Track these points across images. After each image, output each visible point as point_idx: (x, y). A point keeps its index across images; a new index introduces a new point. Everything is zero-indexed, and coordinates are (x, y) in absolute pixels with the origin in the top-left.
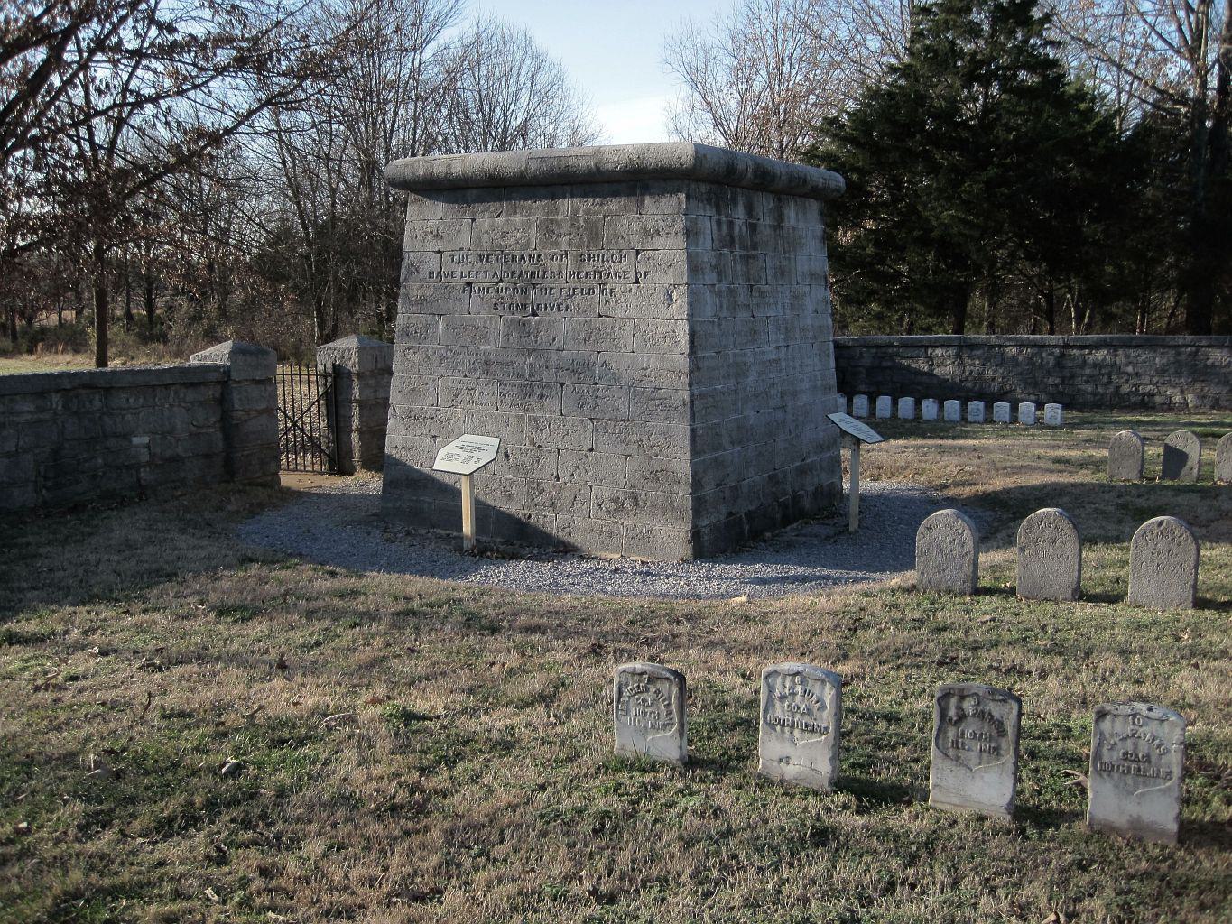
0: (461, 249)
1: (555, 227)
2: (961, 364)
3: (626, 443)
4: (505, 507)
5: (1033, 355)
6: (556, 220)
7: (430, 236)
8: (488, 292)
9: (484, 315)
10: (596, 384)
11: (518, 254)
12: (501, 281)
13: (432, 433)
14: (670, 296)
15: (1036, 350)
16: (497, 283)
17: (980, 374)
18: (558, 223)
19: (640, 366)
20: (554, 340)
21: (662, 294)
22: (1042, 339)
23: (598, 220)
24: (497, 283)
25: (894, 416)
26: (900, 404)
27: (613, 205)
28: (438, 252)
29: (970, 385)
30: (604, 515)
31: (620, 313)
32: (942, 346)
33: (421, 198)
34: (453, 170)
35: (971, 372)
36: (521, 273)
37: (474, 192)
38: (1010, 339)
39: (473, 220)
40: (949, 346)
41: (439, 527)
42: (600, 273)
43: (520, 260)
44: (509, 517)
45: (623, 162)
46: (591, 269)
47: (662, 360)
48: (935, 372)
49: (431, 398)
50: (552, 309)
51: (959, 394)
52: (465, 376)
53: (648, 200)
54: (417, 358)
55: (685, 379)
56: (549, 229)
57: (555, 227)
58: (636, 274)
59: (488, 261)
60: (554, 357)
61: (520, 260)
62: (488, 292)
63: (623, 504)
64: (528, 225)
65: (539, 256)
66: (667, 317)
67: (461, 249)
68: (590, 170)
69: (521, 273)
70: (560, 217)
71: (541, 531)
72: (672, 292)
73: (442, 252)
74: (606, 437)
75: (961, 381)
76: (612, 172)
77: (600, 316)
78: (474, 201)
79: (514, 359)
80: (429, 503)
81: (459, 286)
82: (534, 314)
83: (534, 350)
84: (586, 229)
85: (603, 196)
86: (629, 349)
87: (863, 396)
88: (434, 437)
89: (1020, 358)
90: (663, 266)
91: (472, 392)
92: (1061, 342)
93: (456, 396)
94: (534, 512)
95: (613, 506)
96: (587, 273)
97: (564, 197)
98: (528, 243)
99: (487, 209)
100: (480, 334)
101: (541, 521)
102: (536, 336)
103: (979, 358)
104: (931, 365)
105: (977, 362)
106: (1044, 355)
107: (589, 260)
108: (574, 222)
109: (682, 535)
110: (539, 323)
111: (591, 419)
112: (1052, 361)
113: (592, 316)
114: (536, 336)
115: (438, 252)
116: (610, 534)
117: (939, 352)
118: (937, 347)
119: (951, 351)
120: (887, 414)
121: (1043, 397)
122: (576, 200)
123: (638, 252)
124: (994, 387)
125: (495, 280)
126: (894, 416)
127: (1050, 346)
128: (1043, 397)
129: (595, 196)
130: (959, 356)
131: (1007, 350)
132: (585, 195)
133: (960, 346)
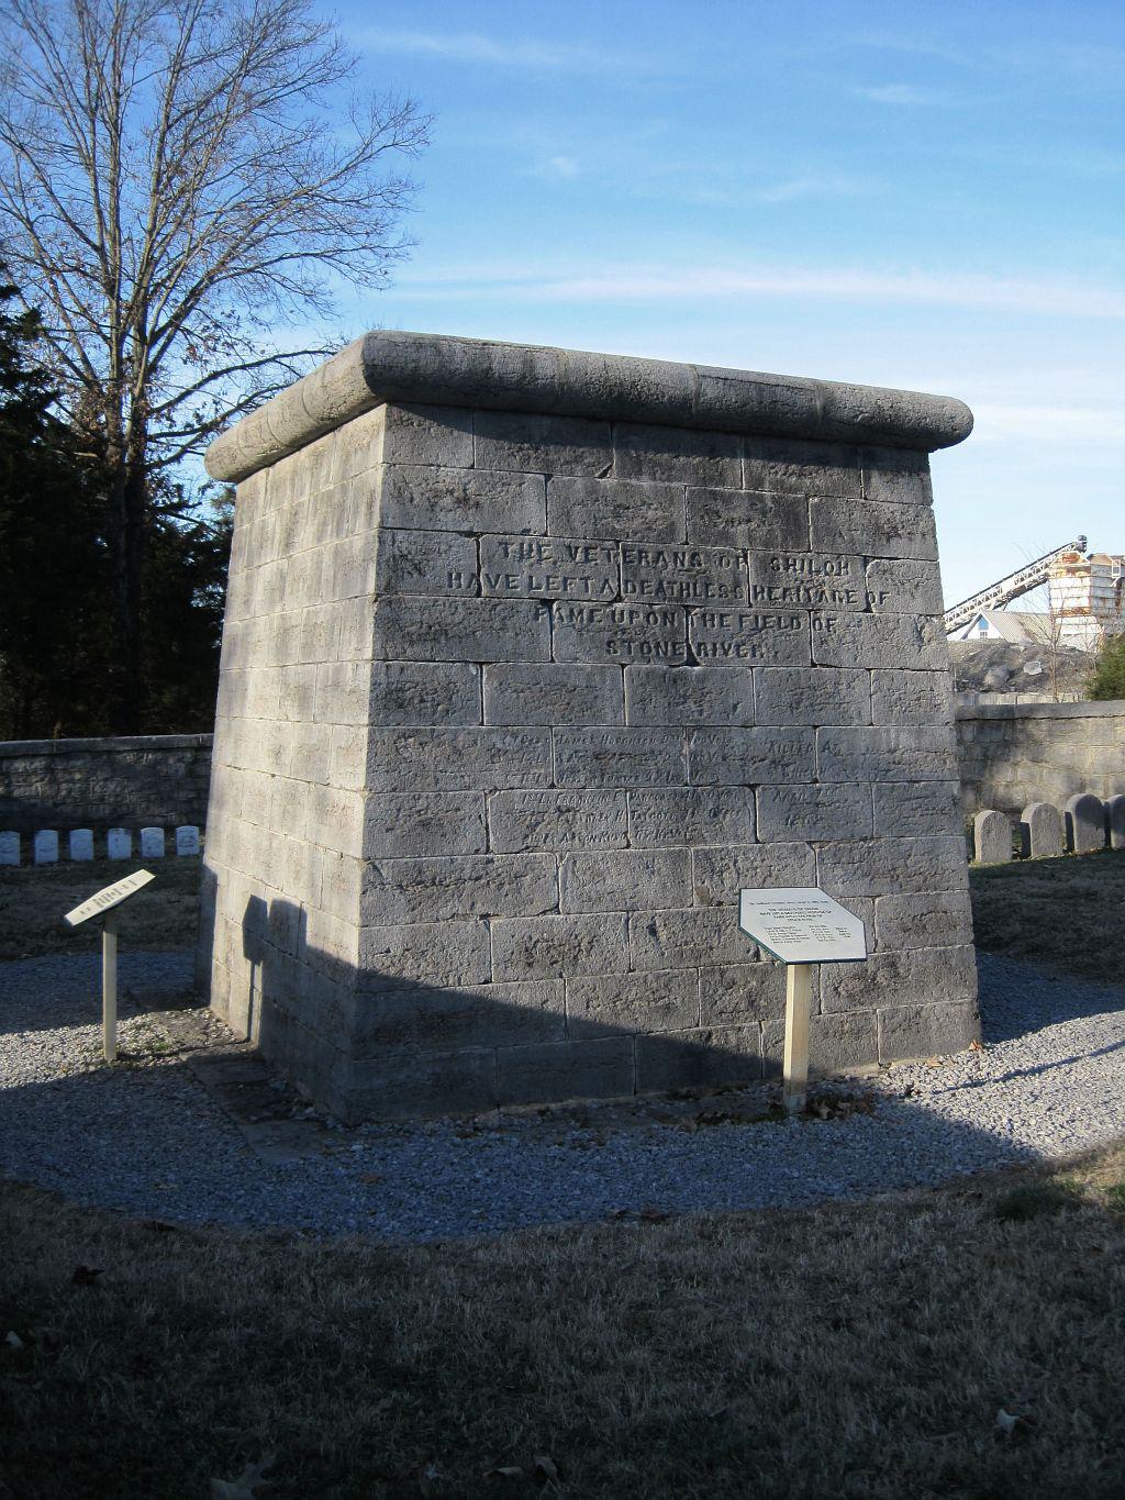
0: (526, 532)
1: (720, 506)
2: (54, 781)
3: (870, 875)
4: (659, 1028)
5: (157, 762)
6: (722, 495)
7: (447, 501)
8: (591, 619)
9: (586, 664)
10: (816, 781)
11: (651, 548)
12: (619, 599)
13: (480, 909)
14: (920, 633)
15: (159, 756)
16: (610, 603)
17: (83, 792)
18: (727, 499)
19: (884, 747)
20: (735, 707)
21: (909, 631)
22: (168, 739)
23: (796, 501)
24: (610, 603)
25: (64, 858)
26: (73, 840)
27: (822, 478)
28: (470, 534)
29: (69, 809)
30: (842, 1002)
31: (846, 658)
32: (25, 756)
33: (416, 419)
34: (539, 371)
35: (70, 791)
36: (661, 584)
37: (546, 422)
38: (124, 742)
39: (548, 477)
40: (35, 756)
41: (512, 1100)
42: (807, 590)
43: (656, 561)
44: (667, 1044)
45: (868, 410)
46: (792, 584)
47: (919, 733)
48: (16, 793)
49: (470, 837)
50: (726, 653)
51: (52, 824)
52: (552, 786)
53: (876, 479)
54: (430, 755)
55: (951, 764)
56: (708, 503)
57: (720, 506)
58: (867, 597)
59: (587, 560)
60: (738, 740)
61: (656, 561)
62: (591, 619)
63: (874, 979)
64: (670, 497)
65: (694, 556)
66: (921, 666)
67: (526, 532)
68: (811, 412)
69: (661, 584)
70: (728, 489)
71: (735, 1058)
72: (922, 628)
73: (477, 535)
74: (839, 871)
75: (55, 804)
76: (847, 424)
77: (814, 665)
78: (547, 441)
79: (657, 745)
80: (482, 1057)
81: (526, 607)
82: (692, 662)
83: (698, 728)
84: (776, 515)
85: (803, 462)
86: (866, 720)
87: (12, 833)
88: (485, 916)
89: (138, 767)
90: (907, 586)
91: (570, 816)
92: (194, 743)
93: (532, 827)
94: (717, 1026)
95: (858, 985)
96: (785, 590)
97: (734, 455)
98: (671, 530)
99: (577, 460)
100: (578, 701)
101: (733, 1040)
102: (698, 703)
103: (80, 772)
104: (8, 785)
105: (78, 776)
106: (171, 761)
107: (787, 569)
108: (754, 500)
109: (965, 1008)
110: (702, 678)
111: (810, 843)
112: (182, 768)
113: (800, 667)
114: (698, 703)
115: (470, 534)
116: (857, 1033)
117: (20, 765)
118: (16, 758)
119: (38, 764)
120: (54, 856)
121: (173, 817)
122: (757, 463)
123: (866, 561)
124: (105, 811)
125: (607, 595)
126: (64, 858)
127: (178, 748)
128: (173, 817)
129: (789, 460)
130: (49, 770)
131: (119, 757)
132: (771, 456)
133: (51, 756)
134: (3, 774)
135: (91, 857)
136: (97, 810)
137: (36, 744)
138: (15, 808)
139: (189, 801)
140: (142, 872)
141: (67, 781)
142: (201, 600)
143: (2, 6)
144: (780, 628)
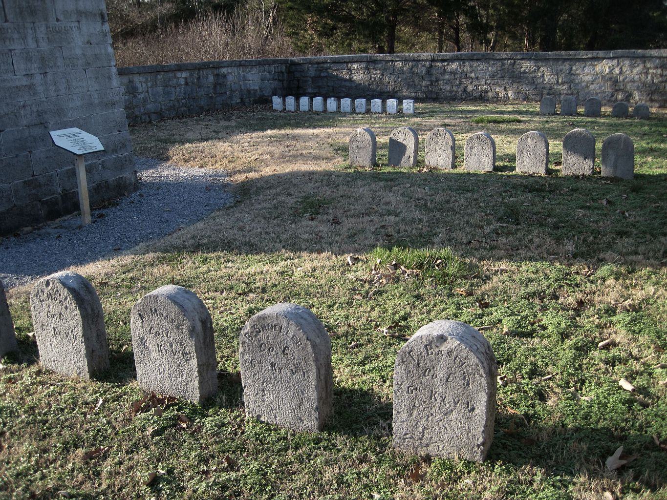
15: (414, 63)
29: (374, 87)
35: (375, 79)
40: (361, 62)
48: (353, 79)
105: (378, 72)
106: (420, 66)
117: (355, 66)
118: (354, 62)
120: (306, 108)
130: (367, 68)
134: (662, 94)
135: (336, 110)
136: (386, 88)
137: (362, 56)
138: (353, 85)
139: (427, 86)
140: (59, 142)
141: (374, 74)
142: (524, 29)
143: (666, 50)
144: (150, 333)
